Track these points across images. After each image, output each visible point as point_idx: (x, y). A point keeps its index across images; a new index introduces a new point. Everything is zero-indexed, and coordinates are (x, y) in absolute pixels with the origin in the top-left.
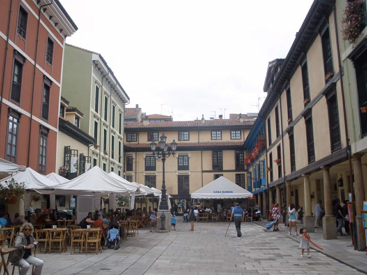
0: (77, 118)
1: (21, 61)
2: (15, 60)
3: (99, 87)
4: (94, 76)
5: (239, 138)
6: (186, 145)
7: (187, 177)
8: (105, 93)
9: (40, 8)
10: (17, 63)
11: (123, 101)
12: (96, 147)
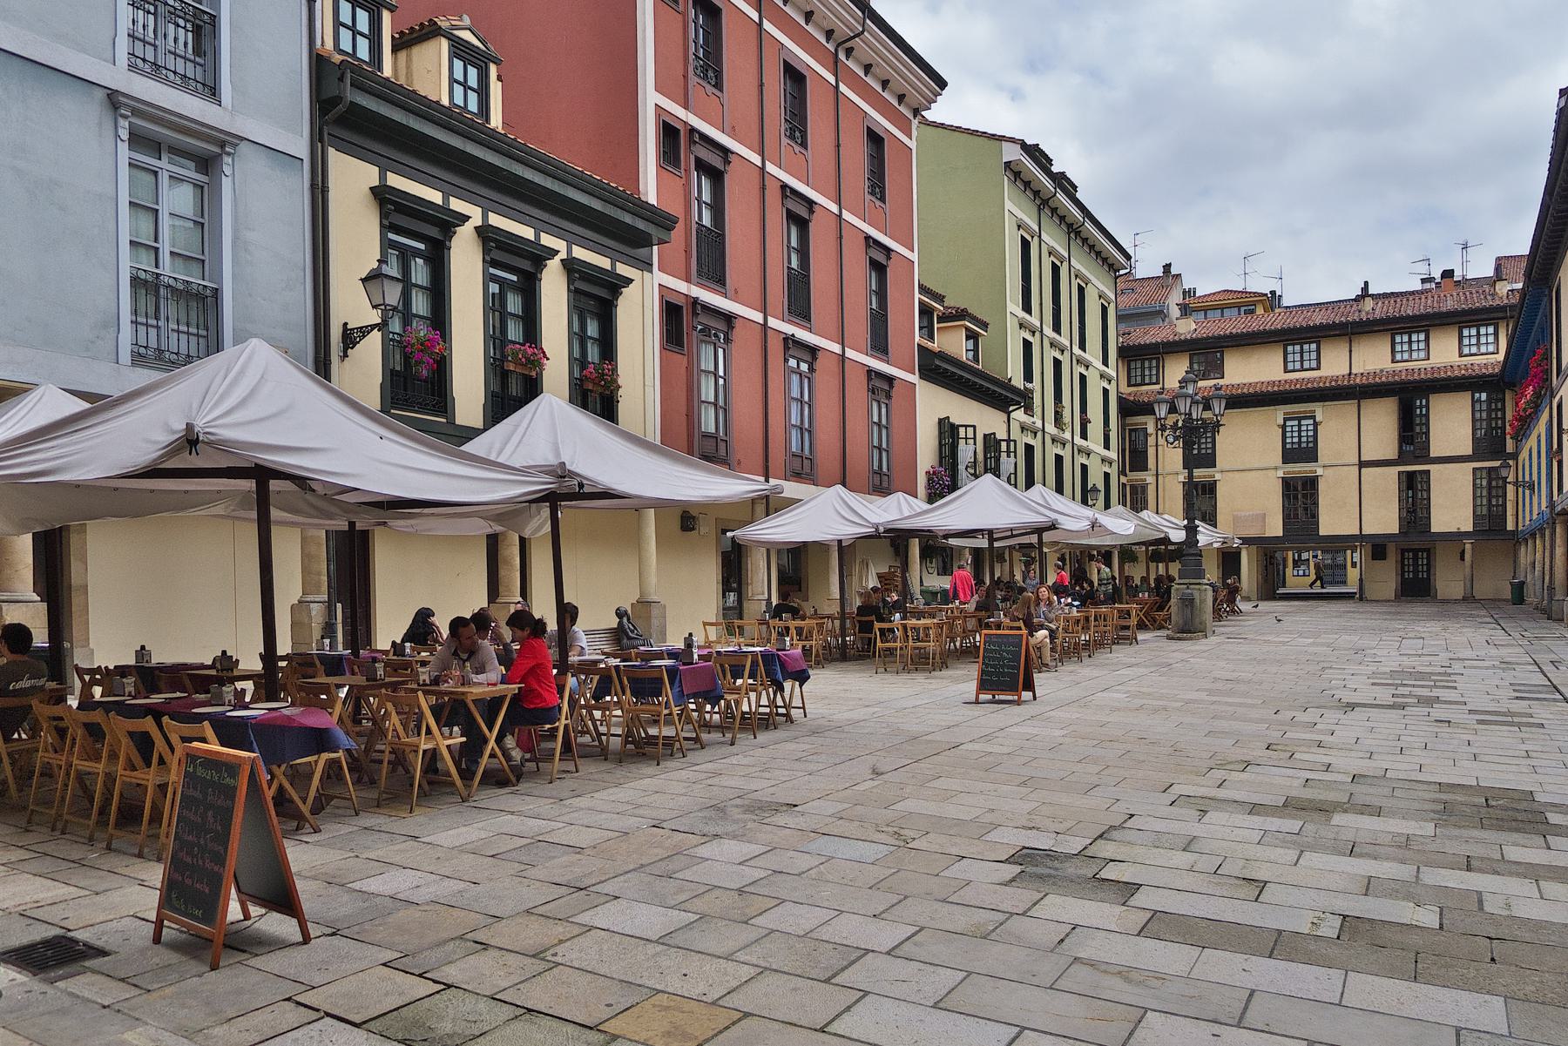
0: (972, 336)
1: (803, 212)
2: (788, 211)
3: (1029, 238)
4: (1016, 209)
5: (1491, 348)
6: (1309, 386)
7: (1311, 483)
8: (1050, 253)
9: (836, 50)
10: (792, 217)
11: (1111, 266)
12: (1029, 410)
